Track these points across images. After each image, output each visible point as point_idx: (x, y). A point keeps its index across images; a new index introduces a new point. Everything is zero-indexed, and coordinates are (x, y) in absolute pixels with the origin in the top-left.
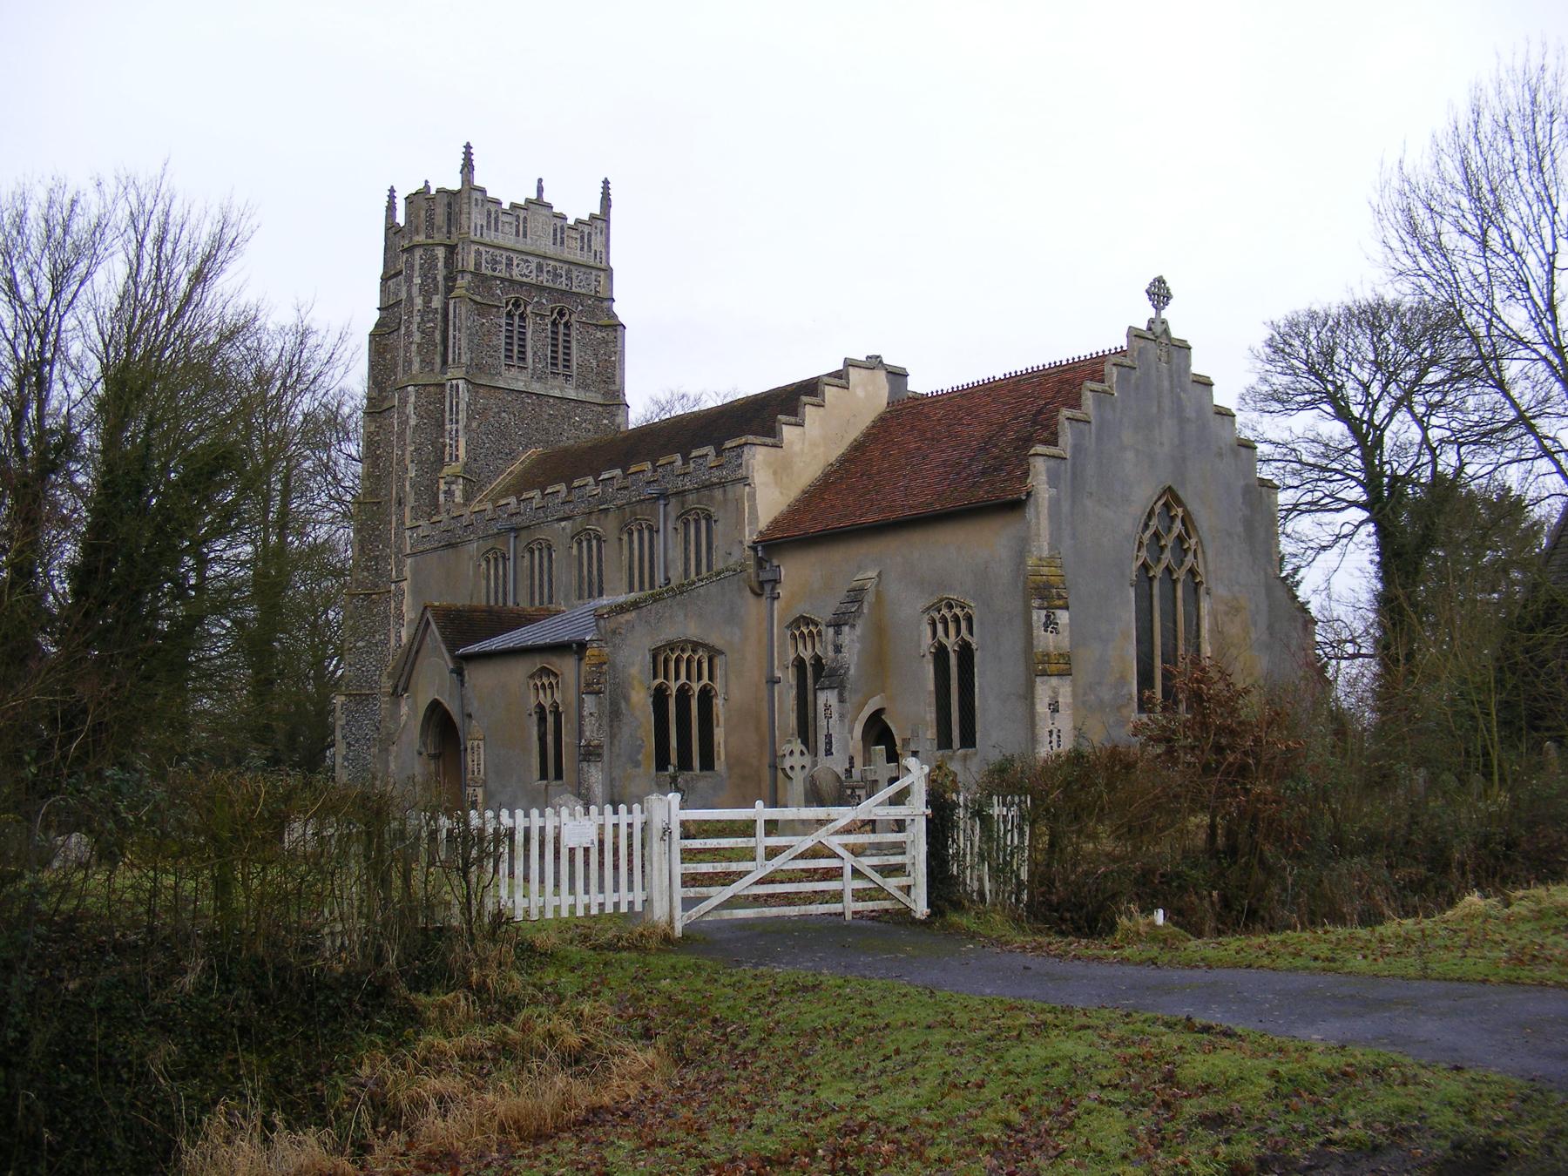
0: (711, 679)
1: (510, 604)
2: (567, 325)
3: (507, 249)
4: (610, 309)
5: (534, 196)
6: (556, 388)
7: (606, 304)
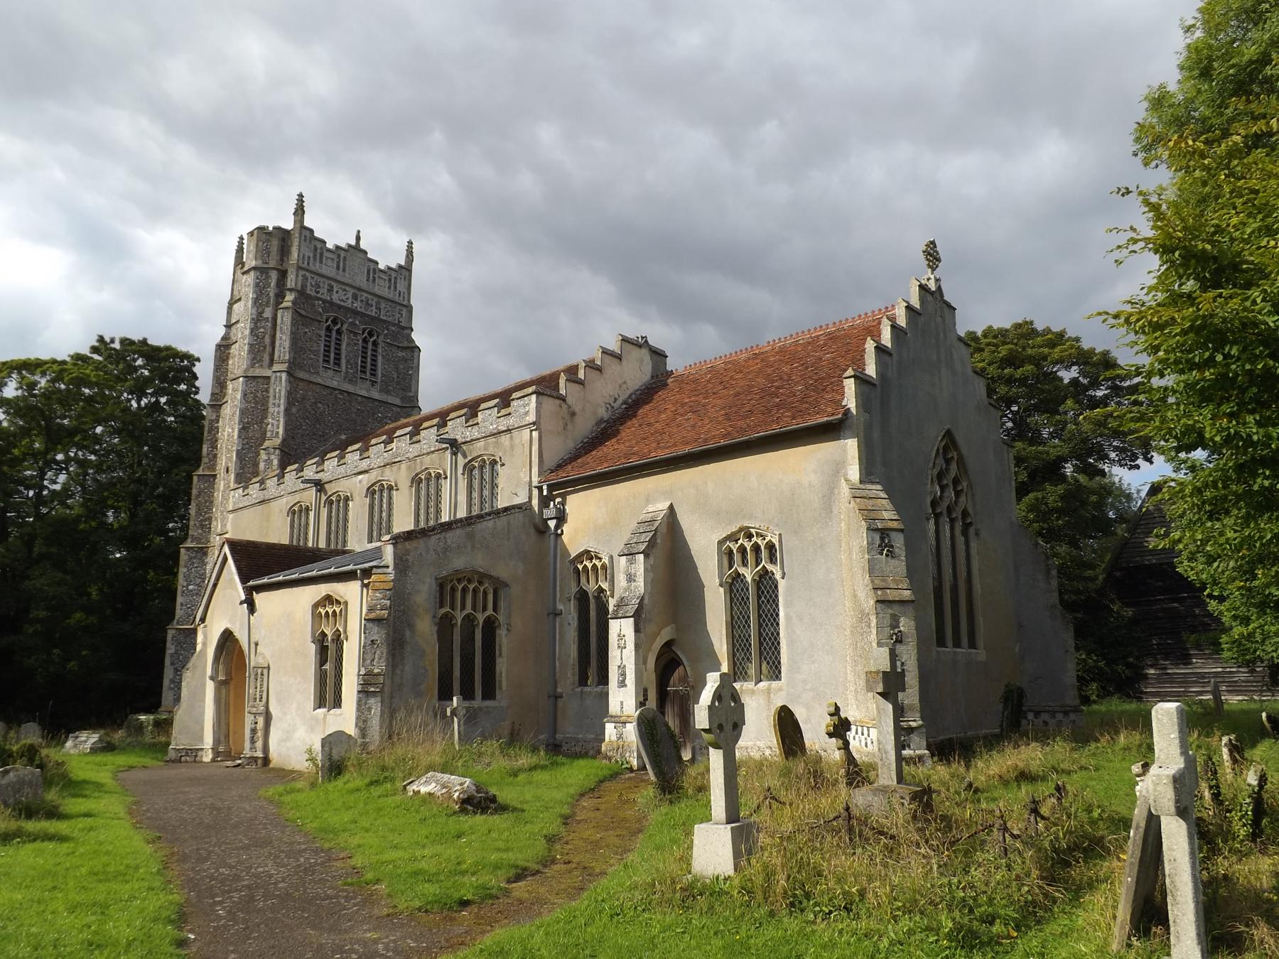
0: (495, 609)
1: (310, 544)
2: (375, 343)
3: (329, 278)
4: (409, 335)
5: (353, 243)
6: (362, 390)
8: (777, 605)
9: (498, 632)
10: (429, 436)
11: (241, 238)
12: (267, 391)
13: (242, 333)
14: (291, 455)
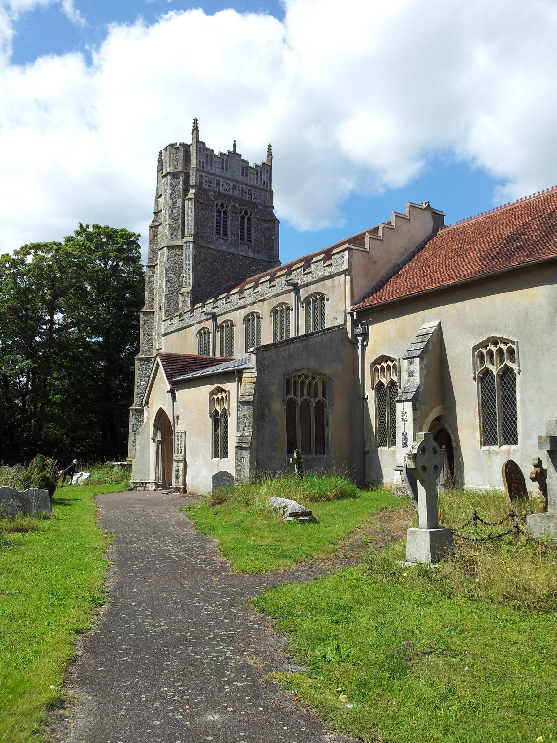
0: (324, 395)
2: (249, 219)
3: (216, 176)
5: (232, 149)
6: (242, 251)
7: (269, 209)
8: (515, 392)
9: (325, 410)
10: (281, 283)
11: (161, 153)
12: (181, 255)
13: (165, 218)
14: (199, 296)
